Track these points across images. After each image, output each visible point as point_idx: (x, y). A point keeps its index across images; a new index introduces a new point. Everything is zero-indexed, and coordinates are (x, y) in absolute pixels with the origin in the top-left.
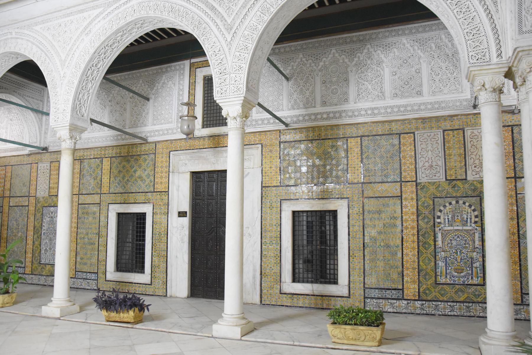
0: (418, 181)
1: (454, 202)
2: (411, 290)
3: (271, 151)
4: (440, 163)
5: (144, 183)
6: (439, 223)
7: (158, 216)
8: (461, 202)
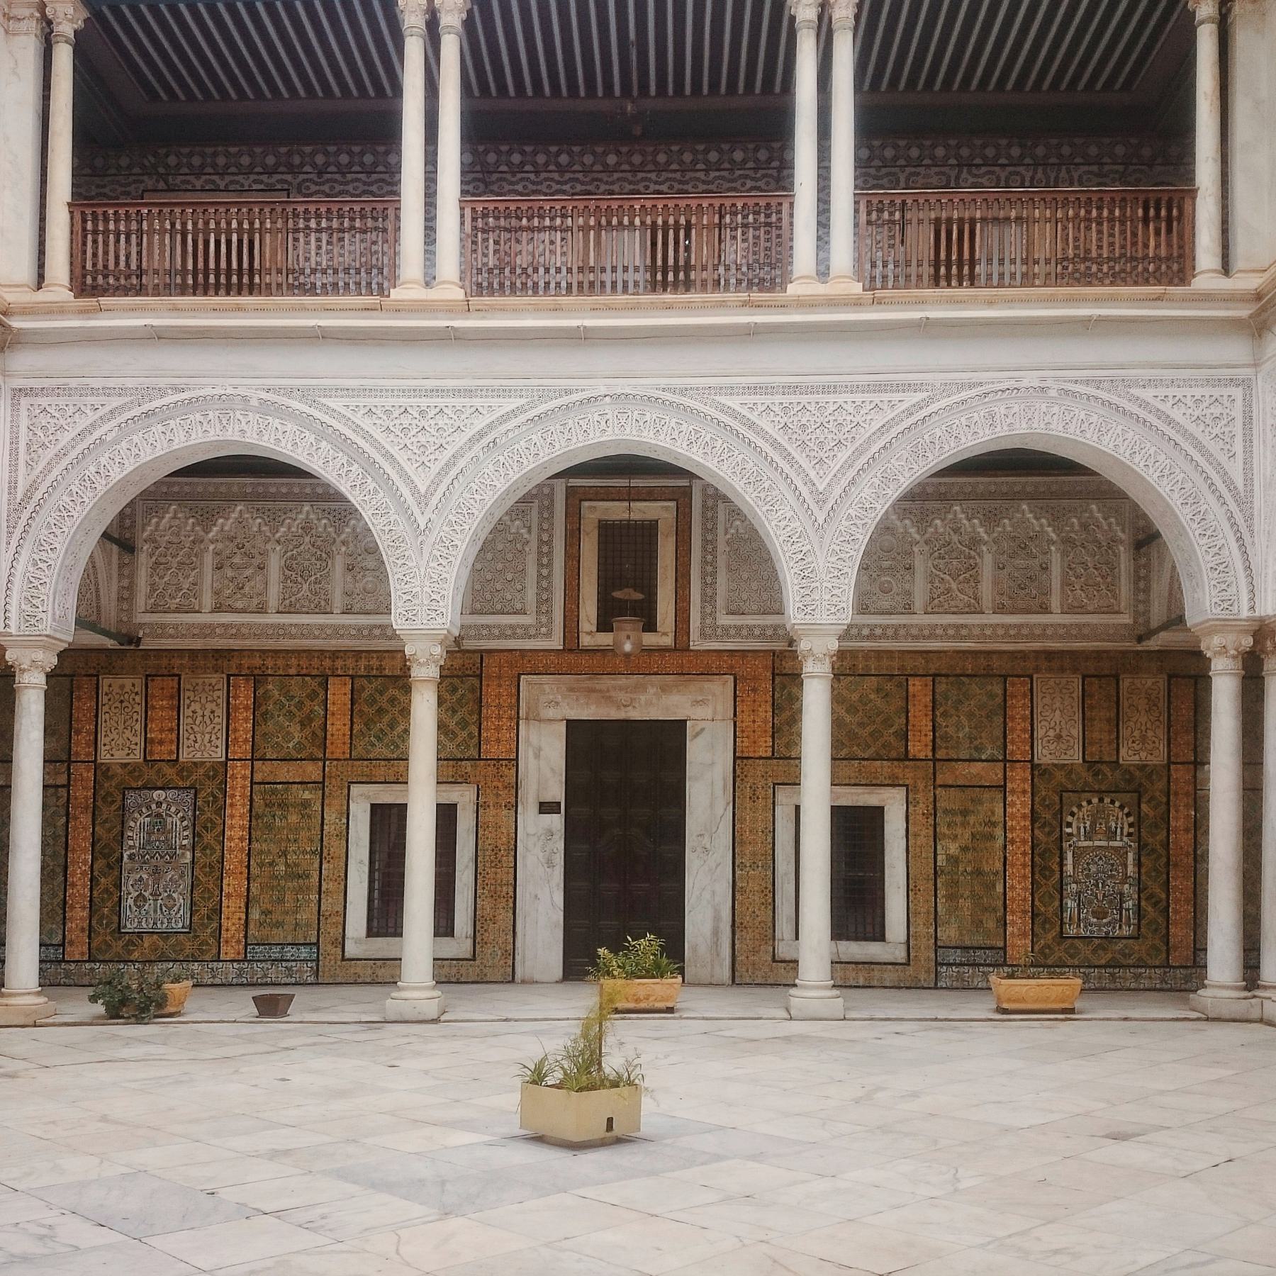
0: (1036, 760)
1: (1095, 800)
3: (754, 690)
5: (451, 740)
6: (1070, 835)
7: (492, 811)
8: (1107, 800)
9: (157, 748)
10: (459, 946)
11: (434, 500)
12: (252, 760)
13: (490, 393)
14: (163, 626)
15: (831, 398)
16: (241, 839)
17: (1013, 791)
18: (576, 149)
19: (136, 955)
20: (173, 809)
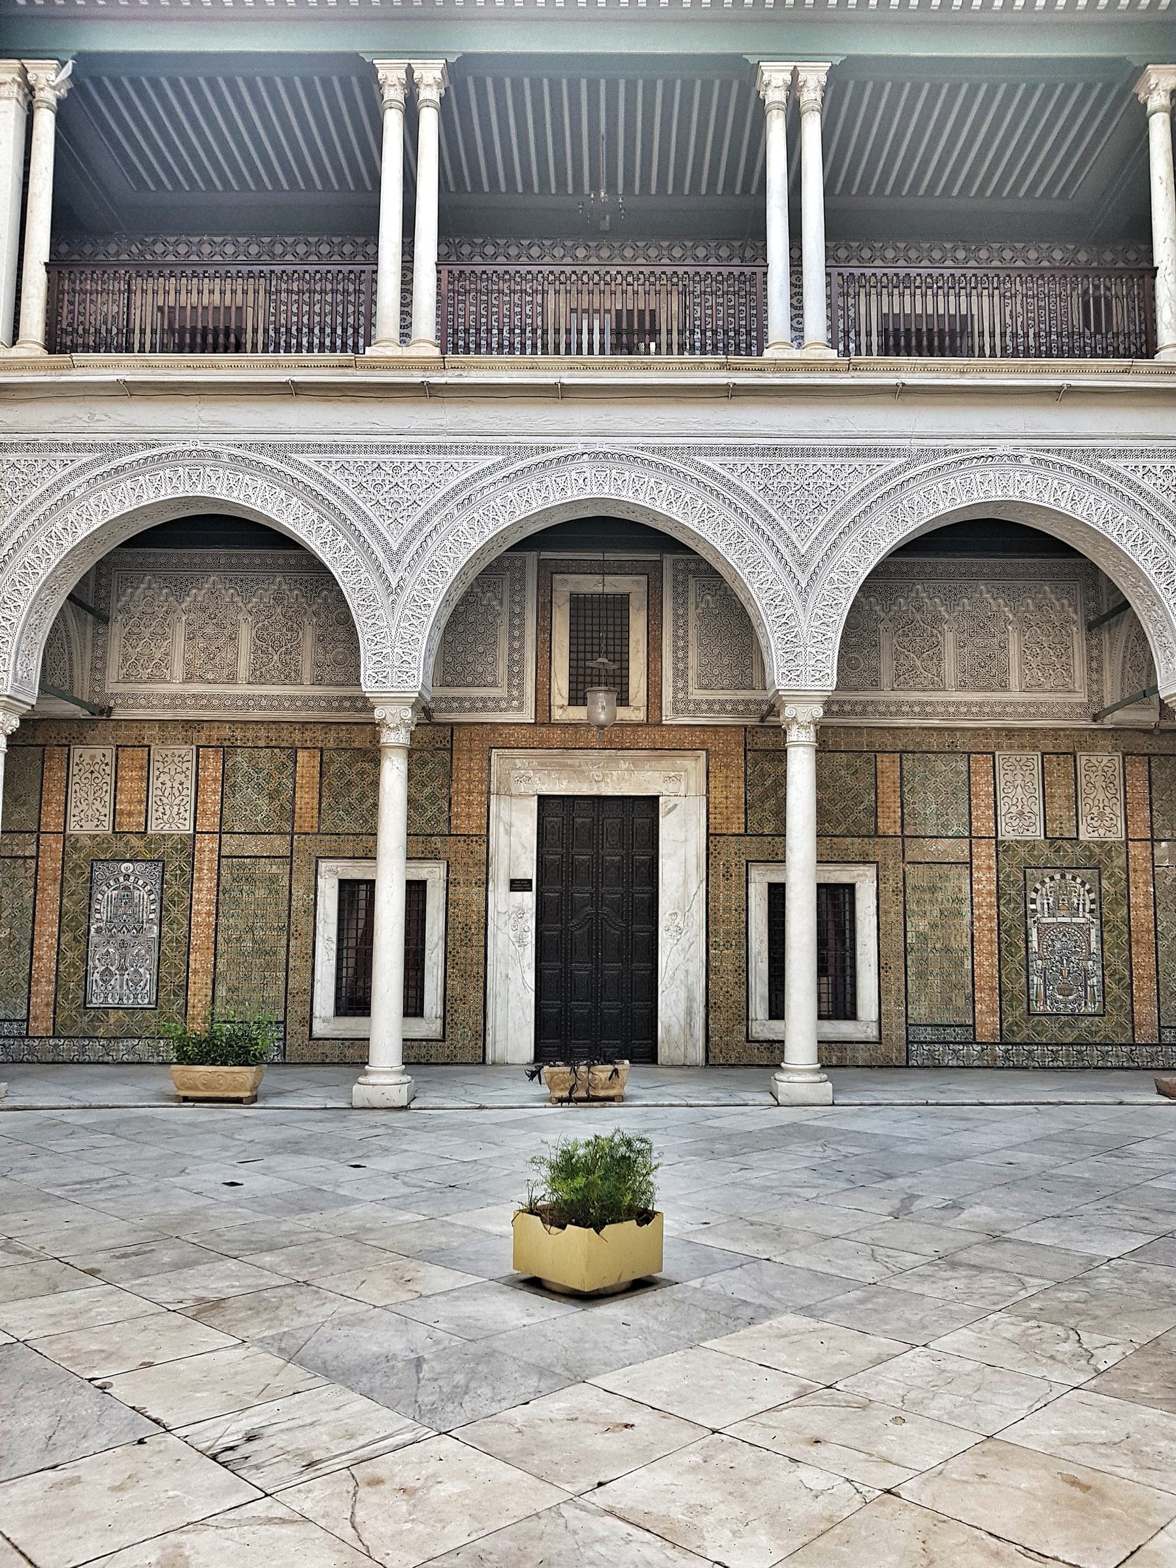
0: (1000, 838)
1: (1057, 877)
2: (988, 1024)
3: (727, 766)
4: (1036, 809)
6: (1033, 911)
7: (461, 889)
8: (1069, 877)
9: (125, 819)
10: (429, 1026)
11: (407, 559)
12: (220, 833)
13: (465, 450)
14: (134, 696)
15: (811, 460)
16: (209, 914)
17: (979, 868)
18: (547, 243)
19: (101, 1032)
20: (140, 882)
